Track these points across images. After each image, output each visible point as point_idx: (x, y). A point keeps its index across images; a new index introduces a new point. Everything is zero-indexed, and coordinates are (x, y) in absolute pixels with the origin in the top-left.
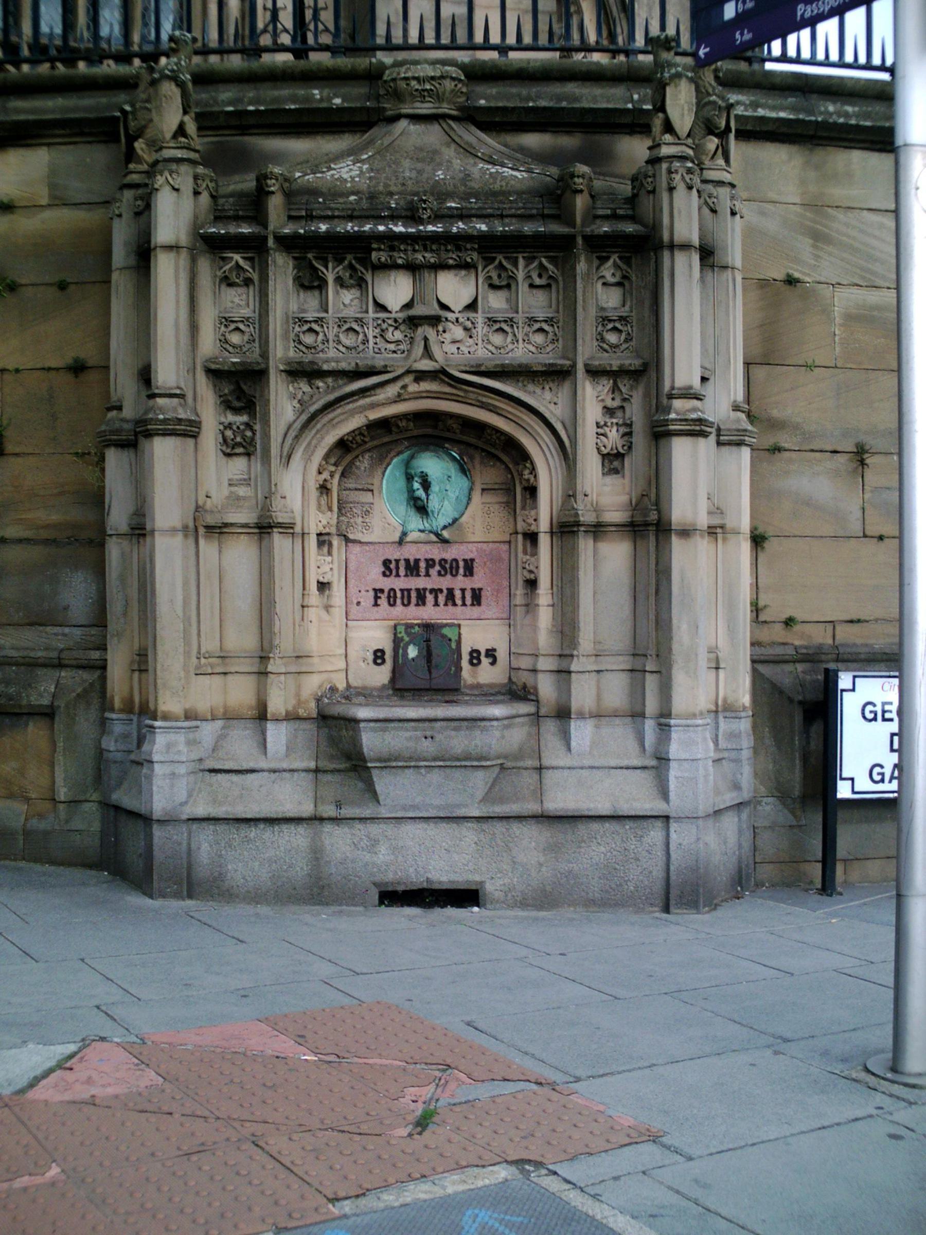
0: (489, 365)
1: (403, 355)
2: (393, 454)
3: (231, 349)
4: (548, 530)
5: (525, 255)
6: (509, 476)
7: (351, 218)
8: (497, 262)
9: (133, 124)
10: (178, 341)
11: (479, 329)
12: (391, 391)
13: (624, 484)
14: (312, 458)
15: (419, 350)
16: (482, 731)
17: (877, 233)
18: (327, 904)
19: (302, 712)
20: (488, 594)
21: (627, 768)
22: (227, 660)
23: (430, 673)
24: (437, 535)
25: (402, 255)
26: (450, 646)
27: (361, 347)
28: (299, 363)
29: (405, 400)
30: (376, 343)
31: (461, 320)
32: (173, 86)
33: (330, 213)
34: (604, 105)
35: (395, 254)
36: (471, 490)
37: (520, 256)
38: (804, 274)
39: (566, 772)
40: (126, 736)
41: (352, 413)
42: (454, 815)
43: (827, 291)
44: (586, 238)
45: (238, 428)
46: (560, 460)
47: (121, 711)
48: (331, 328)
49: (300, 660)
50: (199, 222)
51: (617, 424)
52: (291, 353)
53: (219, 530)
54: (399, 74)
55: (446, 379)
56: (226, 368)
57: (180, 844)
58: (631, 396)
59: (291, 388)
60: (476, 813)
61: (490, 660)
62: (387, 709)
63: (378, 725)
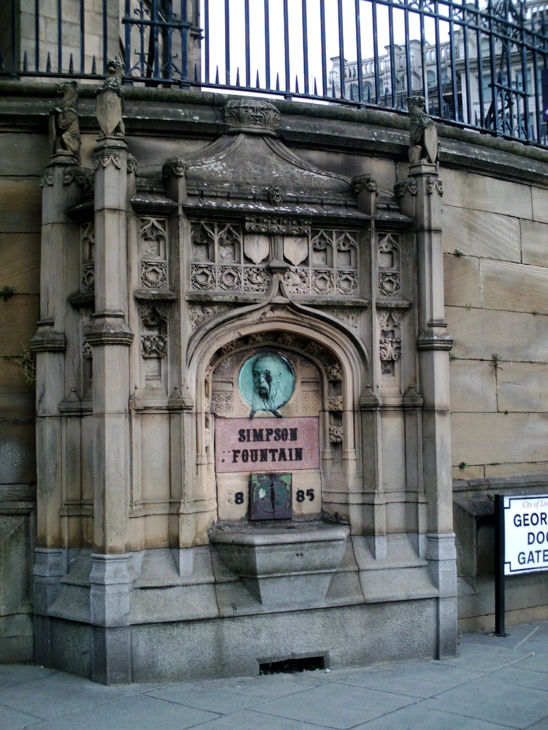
0: (320, 301)
1: (263, 293)
2: (246, 358)
3: (149, 284)
4: (352, 409)
5: (337, 230)
6: (318, 373)
7: (228, 198)
8: (320, 234)
9: (62, 121)
10: (120, 278)
11: (310, 277)
12: (256, 316)
13: (395, 380)
14: (203, 361)
15: (275, 290)
16: (333, 548)
17: (500, 227)
18: (227, 677)
19: (198, 541)
20: (306, 452)
21: (410, 567)
22: (146, 506)
23: (274, 508)
24: (275, 413)
25: (265, 226)
26: (286, 489)
27: (236, 286)
28: (198, 296)
29: (263, 322)
30: (246, 284)
31: (299, 271)
32: (116, 97)
33: (215, 194)
34: (359, 137)
35: (260, 225)
36: (294, 383)
37: (334, 231)
38: (464, 250)
39: (374, 573)
40: (57, 565)
41: (229, 331)
42: (311, 608)
43: (475, 261)
44: (377, 222)
45: (154, 340)
46: (359, 364)
47: (53, 546)
48: (217, 273)
49: (197, 503)
50: (130, 193)
51: (391, 342)
52: (191, 289)
53: (142, 412)
54: (240, 104)
55: (291, 309)
56: (148, 298)
57: (125, 643)
58: (399, 324)
59: (190, 313)
60: (324, 605)
61: (310, 497)
62: (272, 536)
63: (267, 548)
